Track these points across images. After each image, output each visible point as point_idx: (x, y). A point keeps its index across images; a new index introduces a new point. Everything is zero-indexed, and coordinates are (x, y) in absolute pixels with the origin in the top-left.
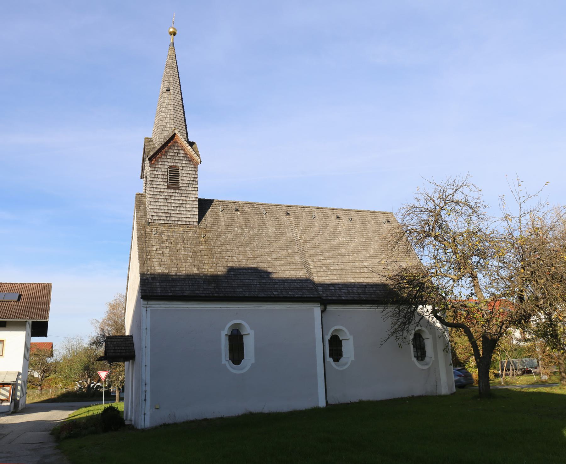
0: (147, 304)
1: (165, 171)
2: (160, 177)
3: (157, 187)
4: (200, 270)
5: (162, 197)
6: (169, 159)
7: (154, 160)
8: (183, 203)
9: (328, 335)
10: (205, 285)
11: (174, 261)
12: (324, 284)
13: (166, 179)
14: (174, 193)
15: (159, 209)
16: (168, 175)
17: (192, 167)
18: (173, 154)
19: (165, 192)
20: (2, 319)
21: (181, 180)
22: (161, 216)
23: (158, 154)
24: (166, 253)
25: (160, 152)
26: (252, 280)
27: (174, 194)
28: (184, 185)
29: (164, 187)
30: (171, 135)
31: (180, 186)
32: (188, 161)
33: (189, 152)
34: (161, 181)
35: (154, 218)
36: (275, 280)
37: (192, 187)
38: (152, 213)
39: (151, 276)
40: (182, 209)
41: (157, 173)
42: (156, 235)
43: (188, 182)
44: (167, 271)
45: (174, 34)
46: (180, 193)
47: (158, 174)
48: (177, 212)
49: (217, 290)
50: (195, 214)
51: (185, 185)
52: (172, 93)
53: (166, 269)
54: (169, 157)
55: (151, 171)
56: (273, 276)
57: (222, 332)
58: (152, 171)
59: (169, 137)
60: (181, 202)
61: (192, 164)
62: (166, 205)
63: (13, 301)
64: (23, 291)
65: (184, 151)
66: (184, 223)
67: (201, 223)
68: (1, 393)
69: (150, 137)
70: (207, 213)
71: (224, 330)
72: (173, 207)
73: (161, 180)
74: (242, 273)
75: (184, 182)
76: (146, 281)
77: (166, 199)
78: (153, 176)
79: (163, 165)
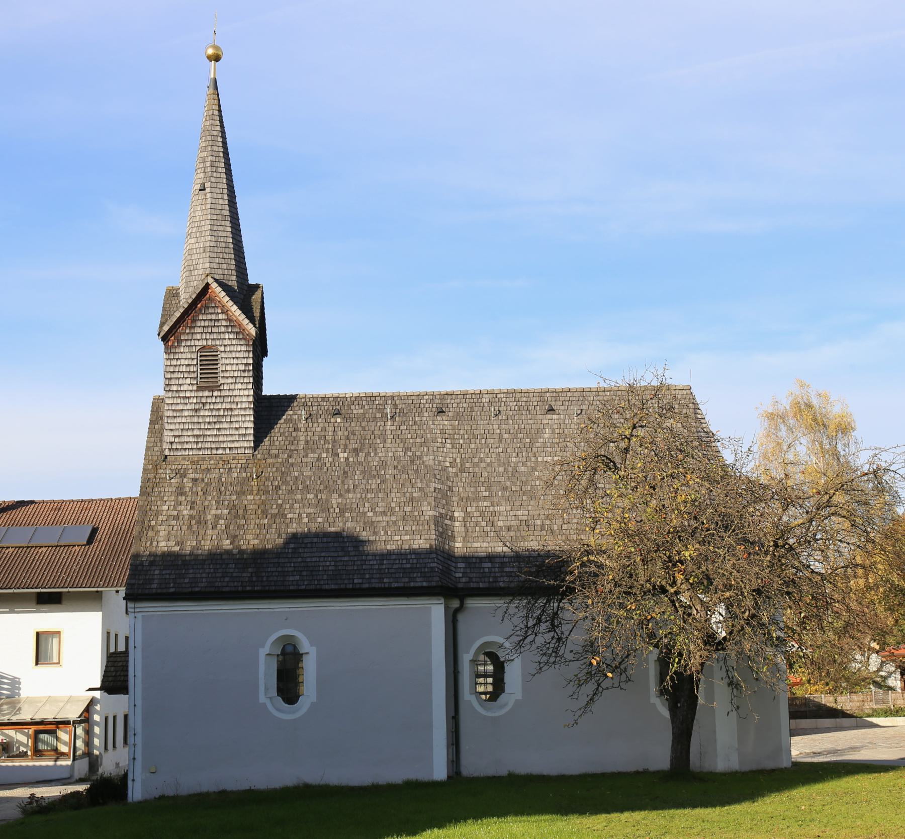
0: (135, 608)
1: (193, 357)
2: (184, 370)
3: (179, 389)
4: (236, 543)
5: (189, 407)
6: (199, 333)
7: (173, 338)
8: (226, 414)
9: (468, 653)
10: (236, 570)
11: (195, 528)
12: (473, 557)
13: (194, 372)
14: (209, 397)
15: (182, 430)
16: (197, 364)
17: (242, 345)
18: (207, 324)
19: (193, 397)
20: (49, 588)
21: (222, 371)
22: (187, 442)
23: (180, 327)
24: (184, 514)
25: (183, 323)
26: (324, 557)
27: (209, 400)
28: (226, 380)
29: (190, 388)
30: (201, 288)
31: (220, 383)
32: (234, 332)
33: (236, 317)
34: (186, 378)
35: (174, 447)
36: (368, 555)
37: (242, 383)
38: (171, 438)
39: (149, 559)
40: (225, 426)
41: (178, 363)
42: (173, 481)
43: (235, 374)
44: (177, 548)
45: (217, 58)
46: (220, 396)
47: (180, 365)
48: (215, 432)
49: (254, 579)
50: (249, 432)
51: (230, 380)
52: (209, 196)
53: (177, 544)
54: (200, 330)
55: (167, 359)
56: (365, 548)
57: (261, 650)
58: (169, 361)
59: (197, 293)
60: (222, 413)
61: (240, 339)
62: (196, 421)
63: (78, 546)
64: (103, 519)
65: (227, 315)
66: (227, 451)
67: (260, 448)
68: (63, 740)
69: (175, 285)
70: (278, 426)
71: (263, 646)
72: (209, 423)
73: (186, 376)
74: (309, 545)
75: (227, 375)
76: (140, 568)
77: (196, 410)
78: (172, 370)
79: (188, 346)
